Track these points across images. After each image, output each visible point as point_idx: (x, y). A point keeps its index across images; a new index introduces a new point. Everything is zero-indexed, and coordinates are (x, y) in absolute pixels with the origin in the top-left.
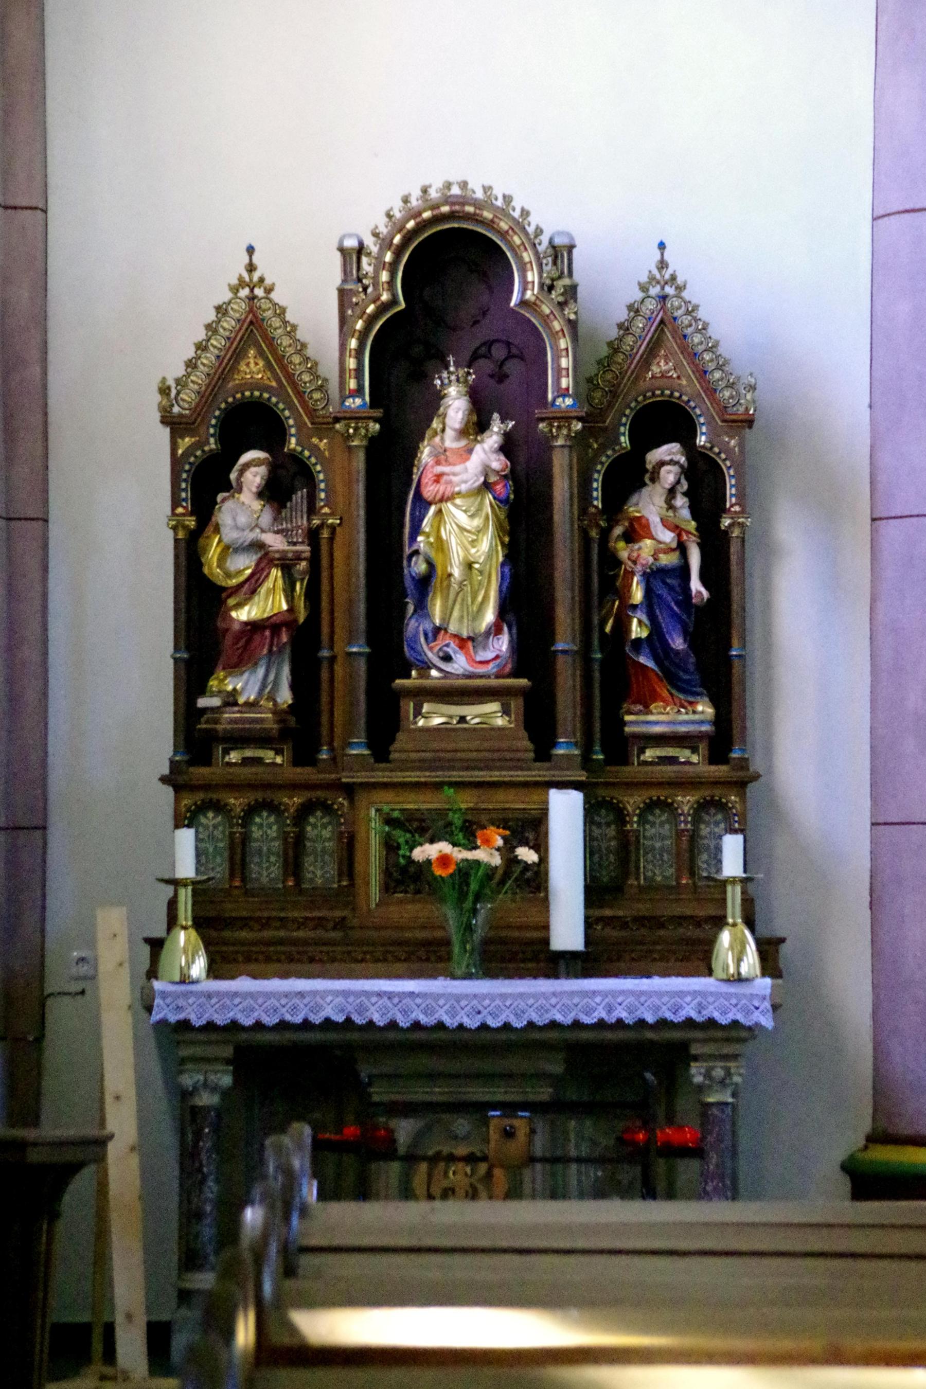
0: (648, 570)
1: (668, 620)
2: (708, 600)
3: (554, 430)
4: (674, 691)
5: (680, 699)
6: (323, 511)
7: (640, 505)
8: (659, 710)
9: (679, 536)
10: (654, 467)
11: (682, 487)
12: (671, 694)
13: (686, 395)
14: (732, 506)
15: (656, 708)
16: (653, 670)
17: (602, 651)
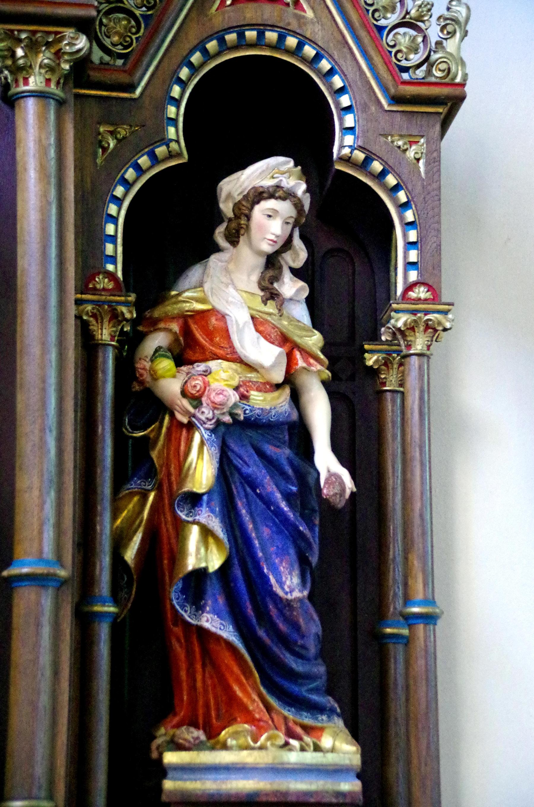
0: (227, 419)
1: (266, 532)
2: (352, 494)
3: (20, 52)
4: (272, 701)
5: (285, 718)
6: (412, 294)
7: (207, 286)
8: (242, 741)
9: (290, 356)
10: (237, 206)
11: (297, 254)
12: (269, 708)
13: (313, 43)
14: (410, 287)
15: (235, 735)
16: (229, 645)
17: (115, 599)
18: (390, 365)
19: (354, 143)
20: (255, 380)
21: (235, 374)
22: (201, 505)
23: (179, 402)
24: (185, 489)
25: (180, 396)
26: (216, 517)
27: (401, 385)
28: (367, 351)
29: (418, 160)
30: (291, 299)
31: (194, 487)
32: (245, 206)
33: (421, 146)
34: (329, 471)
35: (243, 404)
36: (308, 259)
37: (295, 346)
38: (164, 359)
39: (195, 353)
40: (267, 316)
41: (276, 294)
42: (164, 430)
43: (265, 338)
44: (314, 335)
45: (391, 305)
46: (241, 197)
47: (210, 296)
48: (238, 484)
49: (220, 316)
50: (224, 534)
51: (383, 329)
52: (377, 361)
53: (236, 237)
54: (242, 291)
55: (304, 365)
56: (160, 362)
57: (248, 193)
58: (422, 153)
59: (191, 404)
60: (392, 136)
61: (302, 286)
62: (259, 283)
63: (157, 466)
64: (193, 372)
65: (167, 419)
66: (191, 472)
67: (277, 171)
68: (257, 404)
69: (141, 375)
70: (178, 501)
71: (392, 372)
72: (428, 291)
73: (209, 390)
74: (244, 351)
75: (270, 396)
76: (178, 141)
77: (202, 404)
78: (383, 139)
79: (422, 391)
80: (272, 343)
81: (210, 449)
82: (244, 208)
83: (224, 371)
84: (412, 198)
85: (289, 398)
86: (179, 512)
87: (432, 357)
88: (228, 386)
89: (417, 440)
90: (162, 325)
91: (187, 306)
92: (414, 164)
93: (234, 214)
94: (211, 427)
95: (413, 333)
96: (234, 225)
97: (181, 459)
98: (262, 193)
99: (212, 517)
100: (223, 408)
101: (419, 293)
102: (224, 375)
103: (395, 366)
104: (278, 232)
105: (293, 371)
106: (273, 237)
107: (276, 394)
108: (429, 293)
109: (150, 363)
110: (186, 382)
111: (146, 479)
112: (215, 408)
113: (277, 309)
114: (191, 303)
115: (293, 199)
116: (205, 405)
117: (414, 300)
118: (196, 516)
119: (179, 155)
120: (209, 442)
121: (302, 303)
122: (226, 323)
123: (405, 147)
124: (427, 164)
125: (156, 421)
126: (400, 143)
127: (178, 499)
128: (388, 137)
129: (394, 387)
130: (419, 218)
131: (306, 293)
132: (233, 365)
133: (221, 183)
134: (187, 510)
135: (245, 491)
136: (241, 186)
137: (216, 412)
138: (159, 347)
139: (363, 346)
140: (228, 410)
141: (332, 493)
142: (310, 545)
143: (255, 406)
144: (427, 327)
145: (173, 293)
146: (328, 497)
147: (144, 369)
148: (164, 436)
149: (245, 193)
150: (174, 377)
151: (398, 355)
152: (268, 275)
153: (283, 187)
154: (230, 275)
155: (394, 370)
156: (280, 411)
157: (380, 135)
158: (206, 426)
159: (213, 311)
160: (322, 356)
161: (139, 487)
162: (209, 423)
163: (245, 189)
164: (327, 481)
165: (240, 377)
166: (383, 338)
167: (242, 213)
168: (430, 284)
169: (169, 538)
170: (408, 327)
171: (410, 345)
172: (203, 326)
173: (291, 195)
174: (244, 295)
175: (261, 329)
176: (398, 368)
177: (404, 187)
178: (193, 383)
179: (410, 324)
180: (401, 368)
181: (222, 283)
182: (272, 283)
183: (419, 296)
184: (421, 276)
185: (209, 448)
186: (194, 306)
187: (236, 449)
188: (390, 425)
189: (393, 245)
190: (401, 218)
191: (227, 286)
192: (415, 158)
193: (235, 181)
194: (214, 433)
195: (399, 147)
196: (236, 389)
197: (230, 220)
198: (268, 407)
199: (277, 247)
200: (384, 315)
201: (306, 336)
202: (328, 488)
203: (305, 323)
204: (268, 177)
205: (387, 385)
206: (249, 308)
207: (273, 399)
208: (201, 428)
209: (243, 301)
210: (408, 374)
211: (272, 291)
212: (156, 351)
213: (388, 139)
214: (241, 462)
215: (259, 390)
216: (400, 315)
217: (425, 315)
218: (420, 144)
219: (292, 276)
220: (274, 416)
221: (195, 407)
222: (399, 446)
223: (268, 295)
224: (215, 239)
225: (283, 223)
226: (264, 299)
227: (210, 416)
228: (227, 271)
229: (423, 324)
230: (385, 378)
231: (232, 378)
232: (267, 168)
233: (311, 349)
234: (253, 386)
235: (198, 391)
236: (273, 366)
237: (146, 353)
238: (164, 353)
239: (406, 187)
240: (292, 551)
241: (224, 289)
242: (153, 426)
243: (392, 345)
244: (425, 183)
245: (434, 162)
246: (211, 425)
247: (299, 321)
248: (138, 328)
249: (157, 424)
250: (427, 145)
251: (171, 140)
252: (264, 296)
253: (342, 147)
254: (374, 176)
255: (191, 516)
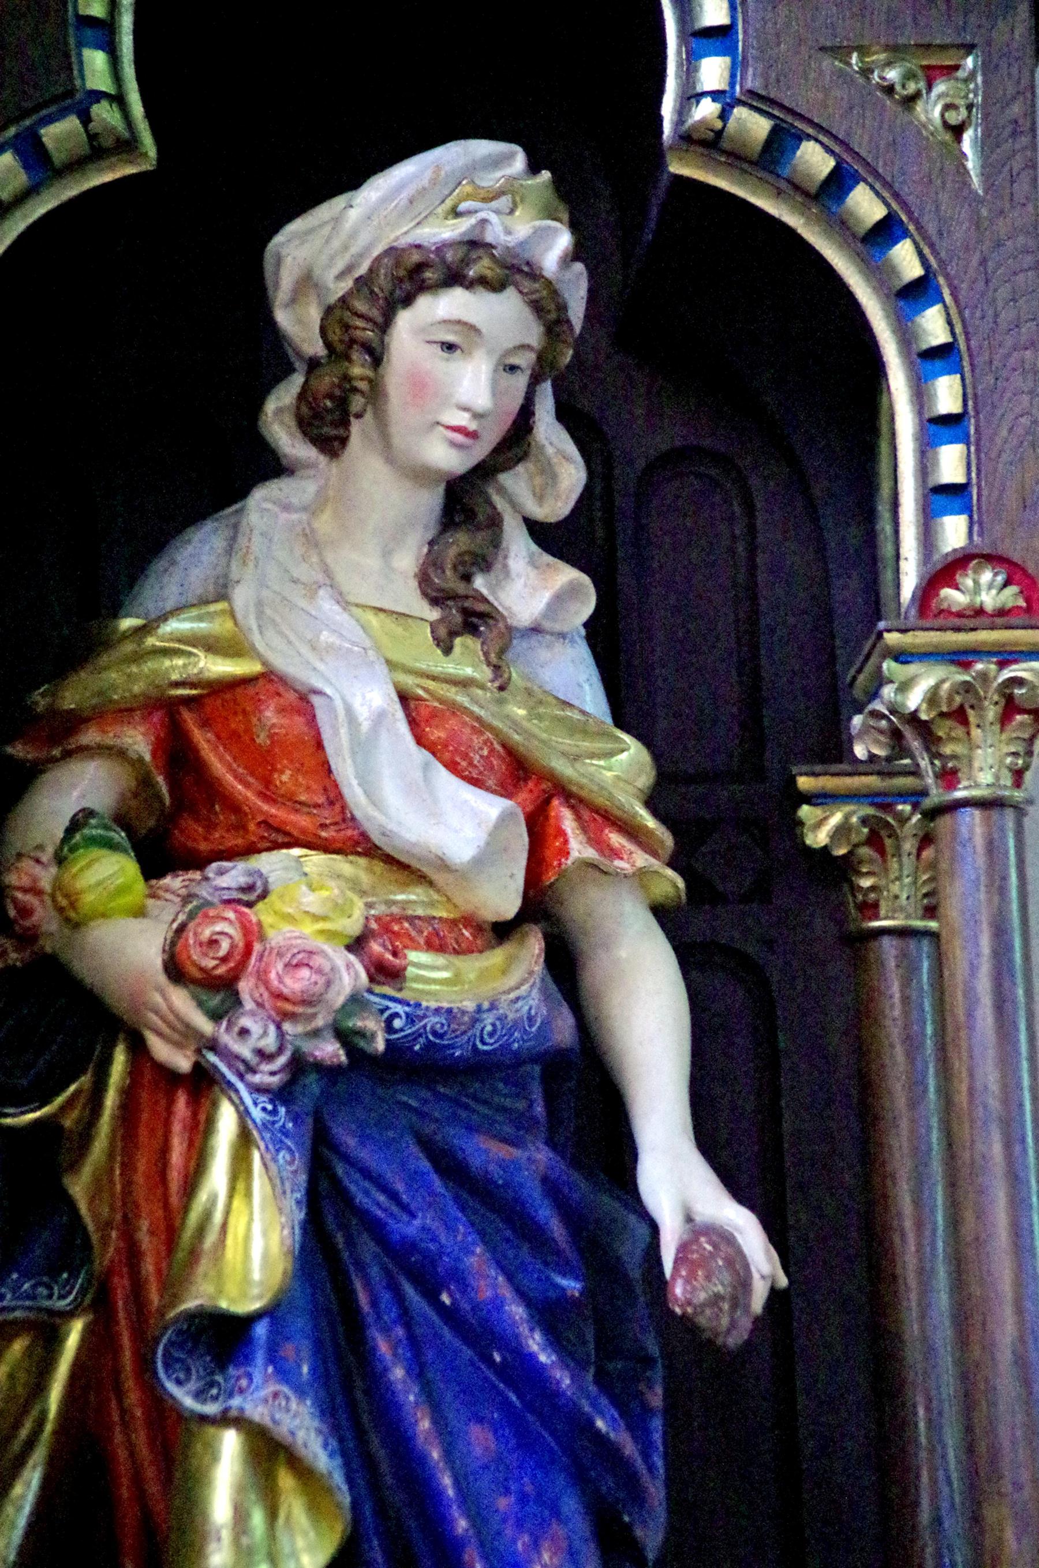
0: (330, 1050)
6: (953, 597)
7: (242, 596)
11: (549, 473)
18: (888, 842)
19: (732, 84)
20: (420, 912)
21: (350, 894)
22: (248, 1359)
23: (158, 998)
24: (190, 1304)
25: (162, 978)
26: (301, 1392)
27: (931, 912)
28: (809, 798)
29: (958, 131)
30: (536, 630)
31: (220, 1292)
32: (361, 316)
33: (966, 81)
34: (689, 1219)
35: (384, 996)
36: (588, 489)
37: (562, 790)
38: (104, 852)
39: (211, 826)
40: (454, 689)
41: (482, 616)
42: (111, 1099)
43: (452, 767)
44: (623, 751)
45: (880, 635)
46: (347, 284)
47: (255, 627)
48: (375, 1271)
49: (291, 697)
50: (331, 1456)
51: (857, 720)
52: (842, 831)
53: (335, 424)
54: (357, 605)
55: (590, 853)
56: (89, 865)
57: (371, 270)
58: (970, 107)
59: (200, 1004)
60: (863, 51)
61: (571, 583)
62: (424, 580)
63: (91, 1227)
64: (204, 892)
65: (120, 1059)
66: (210, 1239)
67: (469, 189)
68: (428, 993)
69: (25, 912)
70: (165, 1349)
71: (896, 866)
72: (1006, 584)
73: (261, 957)
74: (381, 818)
75: (472, 966)
76: (119, 100)
77: (239, 1003)
78: (828, 63)
79: (1000, 931)
80: (476, 782)
81: (275, 1160)
82: (360, 323)
83: (311, 887)
84: (941, 262)
85: (539, 968)
86: (171, 1386)
87: (1031, 809)
88: (330, 935)
89: (994, 1104)
90: (90, 736)
91: (175, 667)
92: (943, 143)
93: (328, 345)
94: (275, 1080)
95: (959, 731)
96: (326, 381)
97: (174, 1200)
98: (421, 267)
99: (288, 1399)
100: (314, 1016)
101: (977, 588)
102: (312, 901)
103: (909, 846)
104: (483, 401)
105: (550, 877)
106: (463, 419)
107: (496, 957)
108: (1013, 589)
109: (53, 870)
110: (182, 929)
111: (54, 1273)
112: (287, 1016)
113: (489, 664)
114: (190, 654)
115: (527, 285)
116: (249, 1005)
117: (960, 615)
118: (231, 1395)
119: (127, 146)
120: (268, 1136)
121: (572, 641)
122: (312, 720)
123: (912, 87)
124: (987, 145)
125: (84, 1072)
126: (893, 75)
127: (164, 1340)
128: (849, 55)
129: (908, 917)
130: (967, 334)
131: (587, 607)
132: (342, 864)
133: (278, 239)
134: (199, 1378)
135: (399, 1298)
136: (346, 248)
137: (287, 1026)
138: (83, 810)
139: (792, 781)
140: (330, 1019)
141: (702, 1296)
142: (637, 1496)
143: (424, 1004)
144: (1010, 708)
145: (127, 623)
146: (689, 1310)
147: (35, 891)
148: (113, 1117)
149: (363, 269)
150: (140, 913)
151: (915, 806)
152: (452, 552)
153: (491, 246)
154: (320, 554)
155: (905, 859)
156: (511, 1016)
157: (823, 49)
158: (257, 1079)
159: (270, 677)
160: (651, 822)
161: (28, 1303)
162: (266, 1067)
163: (361, 256)
164: (683, 1249)
165: (369, 906)
166: (860, 751)
167: (353, 341)
168: (1016, 558)
169: (138, 1480)
170: (945, 709)
171: (954, 772)
172: (235, 735)
173: (520, 271)
174: (374, 620)
175: (436, 734)
176: (918, 855)
177: (911, 228)
178: (207, 933)
179: (950, 699)
180: (928, 853)
181: (295, 581)
182: (467, 578)
183: (978, 600)
184: (981, 534)
185: (268, 1157)
186: (202, 664)
187: (365, 1155)
188: (899, 1052)
189: (884, 429)
190: (906, 336)
191: (312, 591)
192: (946, 124)
193: (326, 230)
194: (286, 1103)
195: (890, 90)
196: (357, 945)
197: (313, 365)
198: (470, 1006)
199: (481, 451)
200: (860, 671)
201: (593, 756)
202: (687, 1281)
203: (588, 708)
204: (440, 210)
205: (883, 912)
206: (392, 665)
207: (484, 975)
208: (240, 1086)
209: (368, 643)
210: (952, 874)
211: (467, 604)
212: (75, 826)
213: (849, 64)
214: (382, 1198)
215: (435, 945)
216: (912, 669)
217: (1002, 664)
218: (961, 74)
219: (534, 547)
220: (491, 1034)
221: (216, 1016)
222: (934, 1122)
223: (458, 618)
224: (264, 432)
225: (495, 371)
226: (442, 632)
227: (270, 1042)
228: (311, 540)
229: (996, 698)
230: (873, 888)
231: (341, 909)
232: (434, 182)
233: (611, 797)
234: (413, 933)
235: (224, 960)
236: (479, 862)
237: (37, 836)
238: (100, 832)
239: (919, 228)
240: (571, 1504)
241: (303, 603)
242: (72, 1088)
243: (891, 774)
244: (984, 212)
245: (1014, 134)
246: (273, 1073)
247: (566, 704)
248: (9, 750)
249: (85, 1080)
250: (984, 75)
251: (97, 96)
252: (441, 620)
253: (690, 97)
254: (806, 194)
255: (215, 1398)
